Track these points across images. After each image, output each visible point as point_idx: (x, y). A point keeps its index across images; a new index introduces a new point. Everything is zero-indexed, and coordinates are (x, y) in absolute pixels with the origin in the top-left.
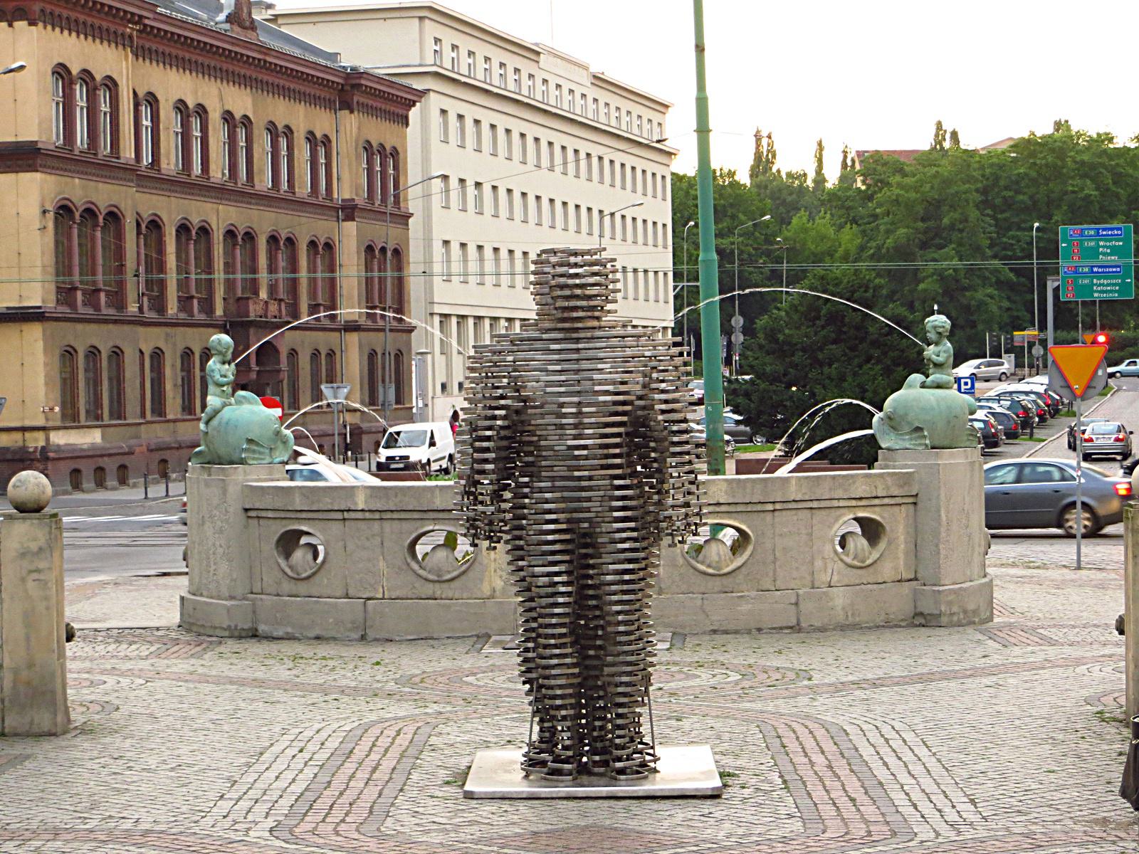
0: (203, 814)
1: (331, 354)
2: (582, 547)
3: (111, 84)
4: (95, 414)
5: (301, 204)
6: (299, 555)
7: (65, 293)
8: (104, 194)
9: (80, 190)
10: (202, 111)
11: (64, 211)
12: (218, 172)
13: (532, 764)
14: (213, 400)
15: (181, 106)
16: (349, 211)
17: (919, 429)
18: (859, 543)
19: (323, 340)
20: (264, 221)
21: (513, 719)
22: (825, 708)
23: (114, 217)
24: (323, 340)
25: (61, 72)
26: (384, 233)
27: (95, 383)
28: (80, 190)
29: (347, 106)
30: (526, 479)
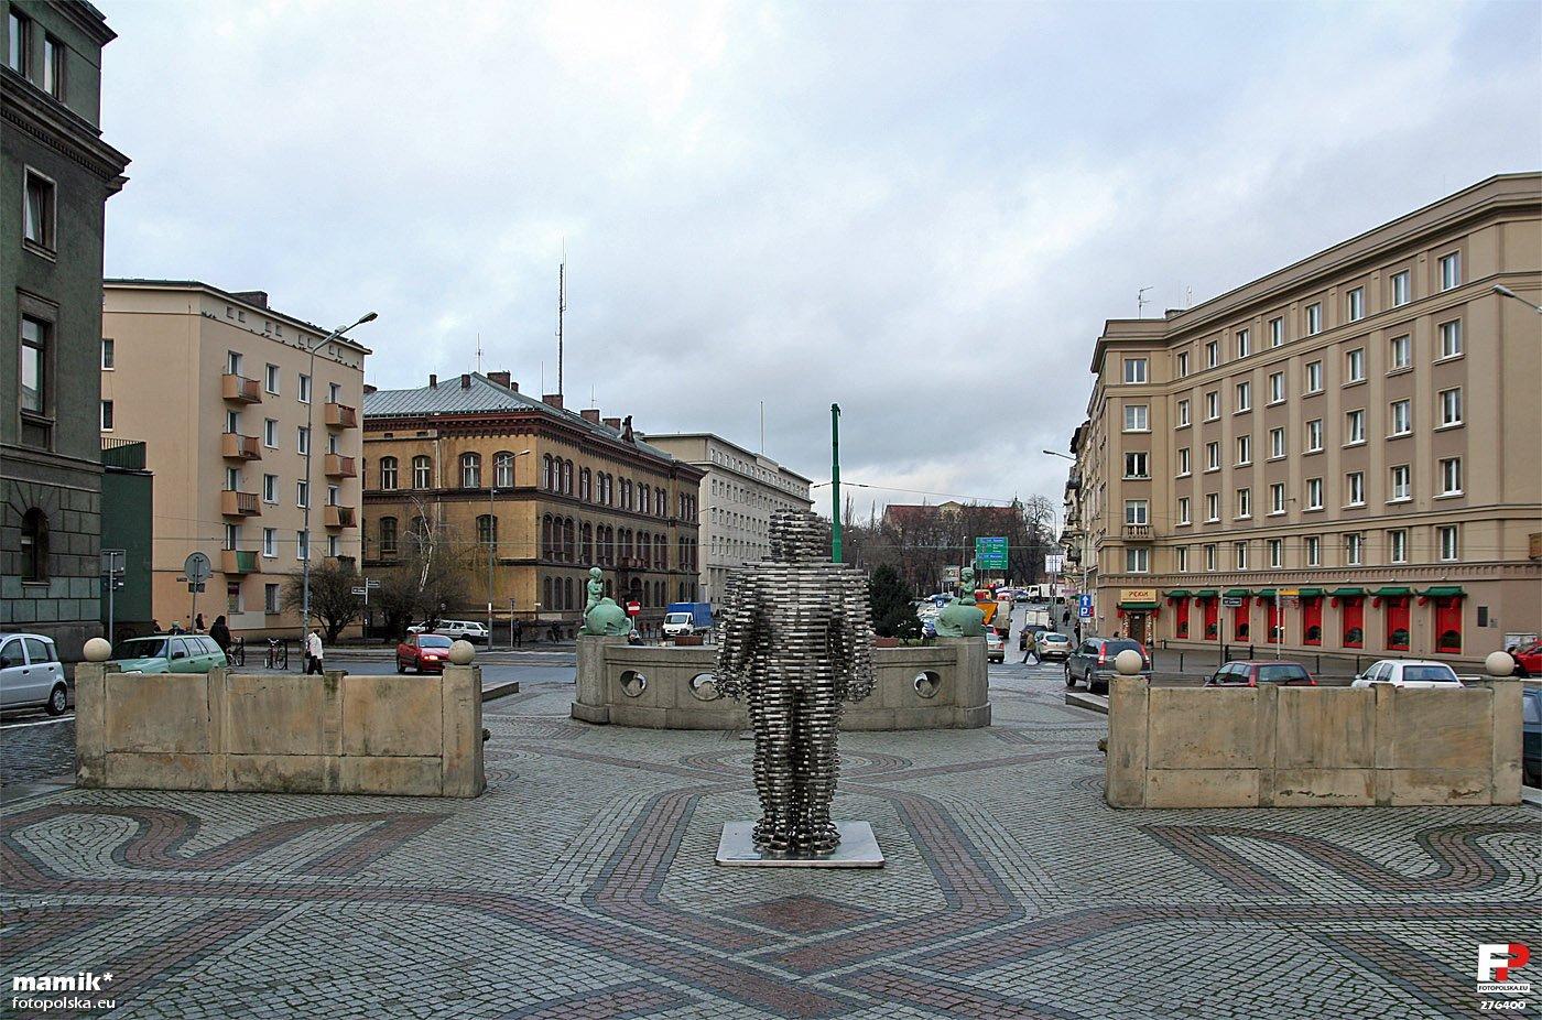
0: (540, 877)
1: (664, 584)
2: (797, 700)
3: (570, 463)
4: (559, 607)
5: (652, 519)
6: (633, 685)
7: (547, 554)
8: (565, 511)
9: (556, 509)
10: (610, 477)
11: (548, 518)
12: (617, 504)
13: (759, 837)
14: (590, 602)
15: (601, 474)
16: (673, 522)
17: (957, 626)
18: (928, 685)
19: (660, 578)
20: (636, 525)
21: (747, 794)
22: (932, 789)
23: (569, 521)
24: (660, 578)
25: (548, 457)
26: (688, 532)
27: (559, 594)
28: (556, 509)
29: (673, 477)
30: (762, 657)
